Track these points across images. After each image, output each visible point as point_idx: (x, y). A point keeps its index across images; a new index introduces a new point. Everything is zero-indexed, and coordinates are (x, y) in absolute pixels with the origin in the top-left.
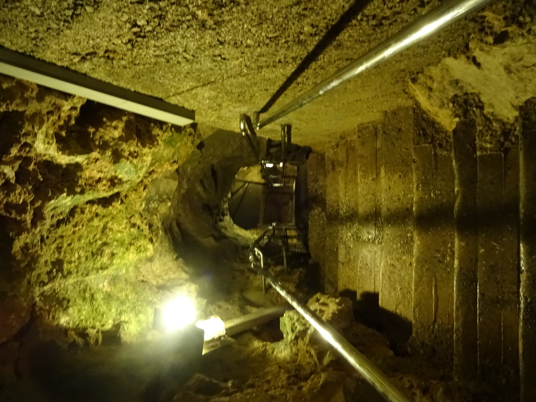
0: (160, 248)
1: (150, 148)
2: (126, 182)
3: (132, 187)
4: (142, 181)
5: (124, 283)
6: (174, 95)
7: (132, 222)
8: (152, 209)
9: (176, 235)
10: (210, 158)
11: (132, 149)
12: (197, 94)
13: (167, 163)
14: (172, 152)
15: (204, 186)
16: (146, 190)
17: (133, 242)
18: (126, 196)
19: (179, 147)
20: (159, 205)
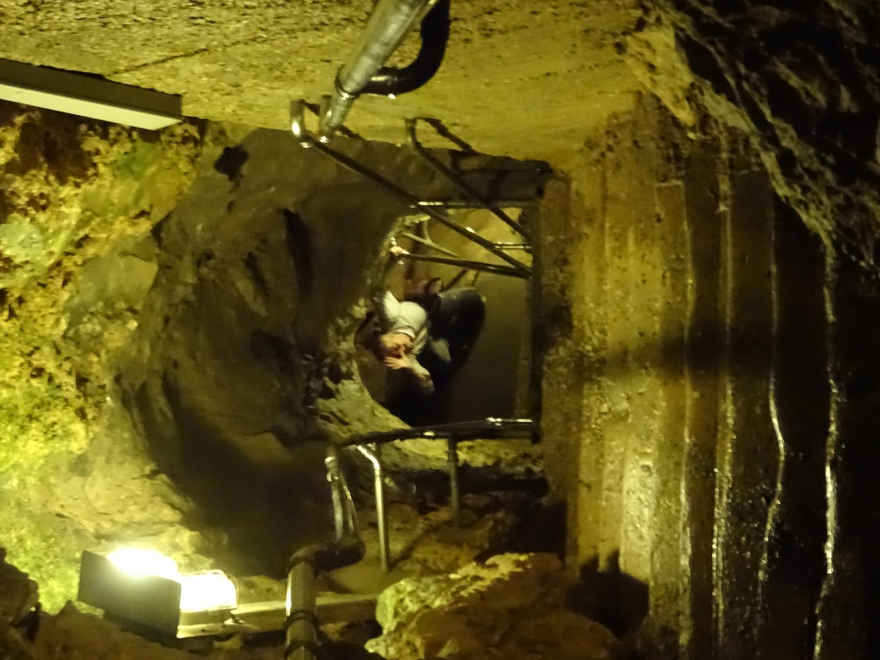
0: (107, 442)
1: (77, 185)
2: (19, 266)
3: (35, 278)
4: (58, 264)
5: (15, 511)
6: (126, 71)
7: (35, 363)
8: (85, 338)
9: (159, 418)
10: (273, 189)
11: (35, 190)
12: (177, 69)
13: (122, 218)
14: (133, 191)
15: (258, 279)
16: (70, 286)
17: (37, 412)
18: (21, 300)
19: (154, 175)
20: (104, 327)
